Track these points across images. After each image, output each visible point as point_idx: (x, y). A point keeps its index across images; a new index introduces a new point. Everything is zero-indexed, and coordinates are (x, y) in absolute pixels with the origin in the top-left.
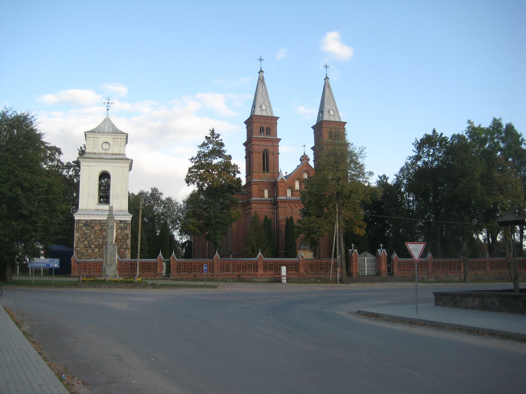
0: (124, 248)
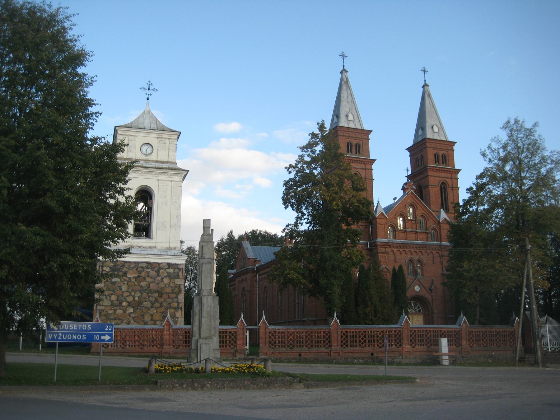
0: (175, 308)
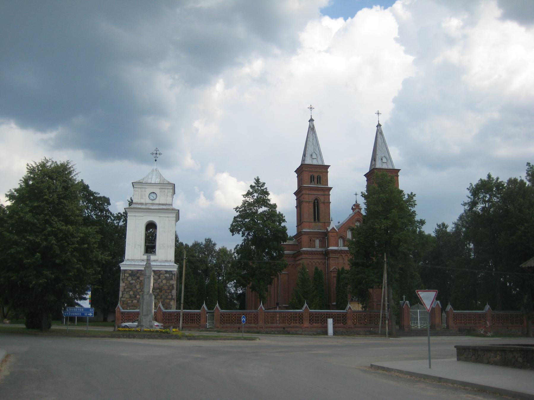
0: (169, 299)
